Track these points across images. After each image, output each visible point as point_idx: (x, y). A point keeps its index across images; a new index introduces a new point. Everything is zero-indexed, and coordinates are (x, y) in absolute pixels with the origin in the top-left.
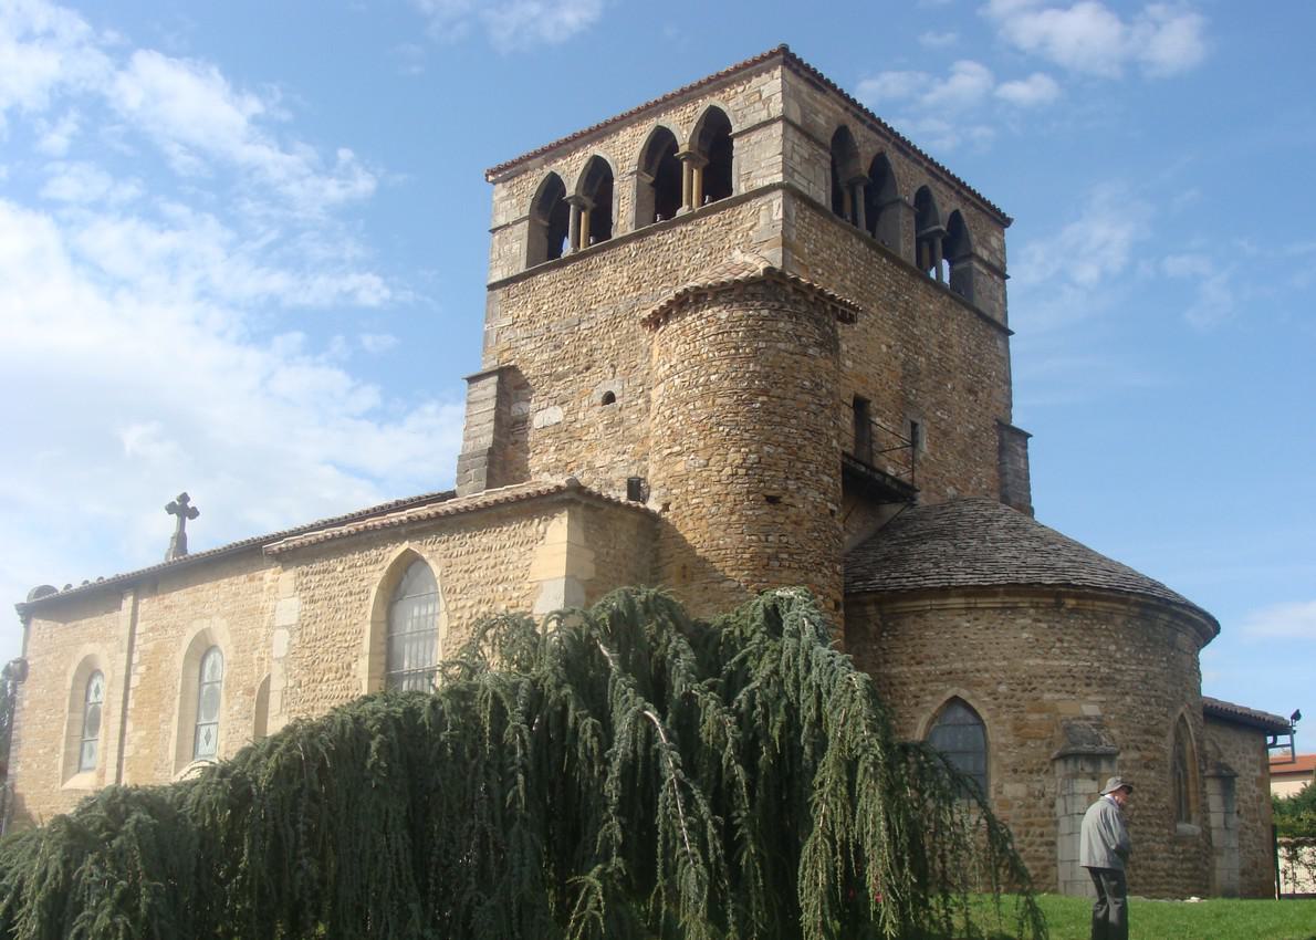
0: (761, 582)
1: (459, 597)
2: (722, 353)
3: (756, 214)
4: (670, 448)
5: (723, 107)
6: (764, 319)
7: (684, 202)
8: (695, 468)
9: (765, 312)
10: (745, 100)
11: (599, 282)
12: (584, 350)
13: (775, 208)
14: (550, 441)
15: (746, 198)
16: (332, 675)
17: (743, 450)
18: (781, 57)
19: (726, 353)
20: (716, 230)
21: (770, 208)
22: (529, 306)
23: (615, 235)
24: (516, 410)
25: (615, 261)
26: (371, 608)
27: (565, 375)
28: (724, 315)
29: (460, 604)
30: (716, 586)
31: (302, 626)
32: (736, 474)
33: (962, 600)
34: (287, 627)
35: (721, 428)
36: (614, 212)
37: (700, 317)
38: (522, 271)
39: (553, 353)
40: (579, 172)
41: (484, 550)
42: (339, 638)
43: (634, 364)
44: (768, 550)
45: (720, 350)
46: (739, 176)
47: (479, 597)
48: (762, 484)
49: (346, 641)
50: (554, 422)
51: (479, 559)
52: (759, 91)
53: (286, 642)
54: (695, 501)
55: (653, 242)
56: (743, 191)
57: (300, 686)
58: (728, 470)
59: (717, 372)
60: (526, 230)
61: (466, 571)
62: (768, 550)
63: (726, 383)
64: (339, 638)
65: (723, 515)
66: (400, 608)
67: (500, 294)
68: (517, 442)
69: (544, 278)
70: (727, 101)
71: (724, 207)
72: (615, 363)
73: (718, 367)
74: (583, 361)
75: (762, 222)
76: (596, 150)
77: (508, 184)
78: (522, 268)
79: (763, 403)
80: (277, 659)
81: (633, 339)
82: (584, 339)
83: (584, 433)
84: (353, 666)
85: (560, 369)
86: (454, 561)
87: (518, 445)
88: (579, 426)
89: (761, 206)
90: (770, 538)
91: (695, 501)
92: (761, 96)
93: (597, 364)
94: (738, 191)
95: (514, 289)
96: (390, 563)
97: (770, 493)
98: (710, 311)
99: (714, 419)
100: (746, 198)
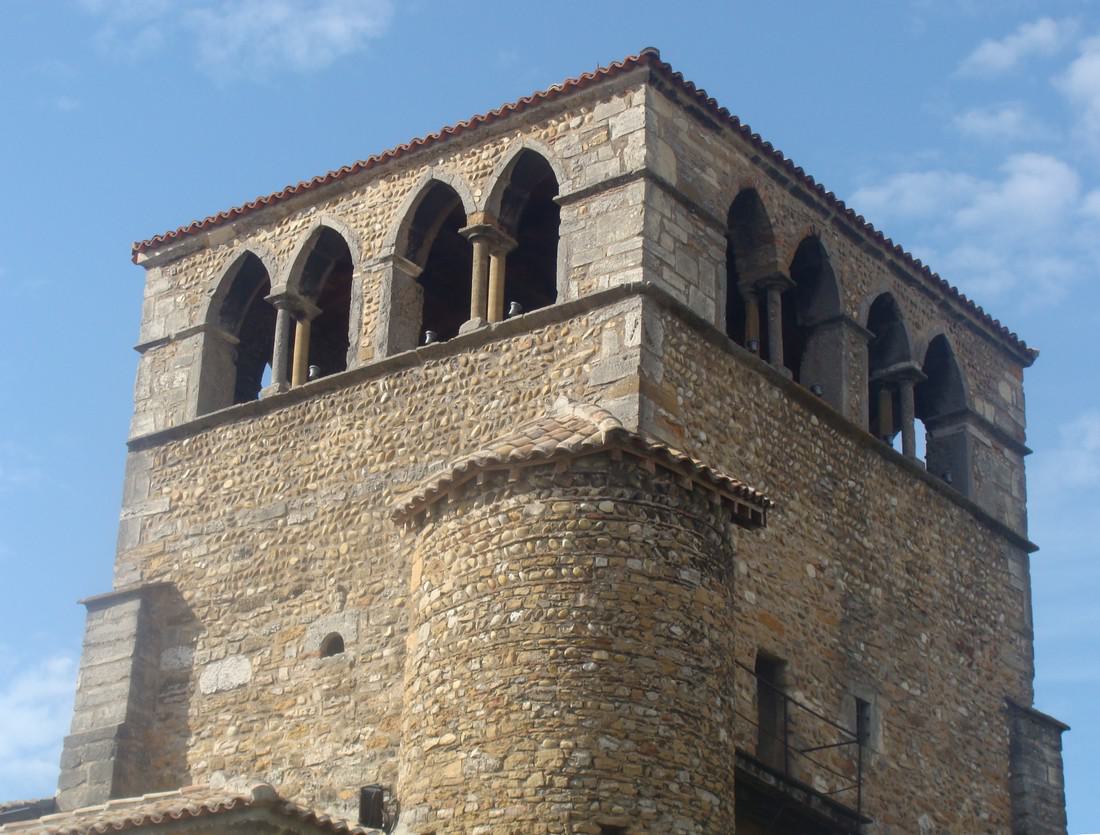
3: (596, 336)
4: (436, 735)
6: (606, 517)
9: (607, 506)
10: (582, 140)
11: (321, 444)
19: (538, 574)
23: (353, 364)
27: (258, 602)
28: (536, 508)
32: (551, 784)
35: (526, 705)
36: (353, 325)
37: (496, 511)
39: (238, 563)
40: (294, 254)
43: (378, 586)
55: (418, 378)
56: (574, 295)
59: (521, 607)
60: (199, 350)
67: (149, 457)
68: (168, 716)
69: (228, 434)
71: (541, 322)
72: (345, 584)
74: (289, 579)
76: (324, 216)
77: (171, 269)
78: (189, 413)
79: (600, 663)
82: (293, 541)
89: (606, 321)
92: (609, 134)
93: (314, 585)
95: (175, 451)
98: (512, 502)
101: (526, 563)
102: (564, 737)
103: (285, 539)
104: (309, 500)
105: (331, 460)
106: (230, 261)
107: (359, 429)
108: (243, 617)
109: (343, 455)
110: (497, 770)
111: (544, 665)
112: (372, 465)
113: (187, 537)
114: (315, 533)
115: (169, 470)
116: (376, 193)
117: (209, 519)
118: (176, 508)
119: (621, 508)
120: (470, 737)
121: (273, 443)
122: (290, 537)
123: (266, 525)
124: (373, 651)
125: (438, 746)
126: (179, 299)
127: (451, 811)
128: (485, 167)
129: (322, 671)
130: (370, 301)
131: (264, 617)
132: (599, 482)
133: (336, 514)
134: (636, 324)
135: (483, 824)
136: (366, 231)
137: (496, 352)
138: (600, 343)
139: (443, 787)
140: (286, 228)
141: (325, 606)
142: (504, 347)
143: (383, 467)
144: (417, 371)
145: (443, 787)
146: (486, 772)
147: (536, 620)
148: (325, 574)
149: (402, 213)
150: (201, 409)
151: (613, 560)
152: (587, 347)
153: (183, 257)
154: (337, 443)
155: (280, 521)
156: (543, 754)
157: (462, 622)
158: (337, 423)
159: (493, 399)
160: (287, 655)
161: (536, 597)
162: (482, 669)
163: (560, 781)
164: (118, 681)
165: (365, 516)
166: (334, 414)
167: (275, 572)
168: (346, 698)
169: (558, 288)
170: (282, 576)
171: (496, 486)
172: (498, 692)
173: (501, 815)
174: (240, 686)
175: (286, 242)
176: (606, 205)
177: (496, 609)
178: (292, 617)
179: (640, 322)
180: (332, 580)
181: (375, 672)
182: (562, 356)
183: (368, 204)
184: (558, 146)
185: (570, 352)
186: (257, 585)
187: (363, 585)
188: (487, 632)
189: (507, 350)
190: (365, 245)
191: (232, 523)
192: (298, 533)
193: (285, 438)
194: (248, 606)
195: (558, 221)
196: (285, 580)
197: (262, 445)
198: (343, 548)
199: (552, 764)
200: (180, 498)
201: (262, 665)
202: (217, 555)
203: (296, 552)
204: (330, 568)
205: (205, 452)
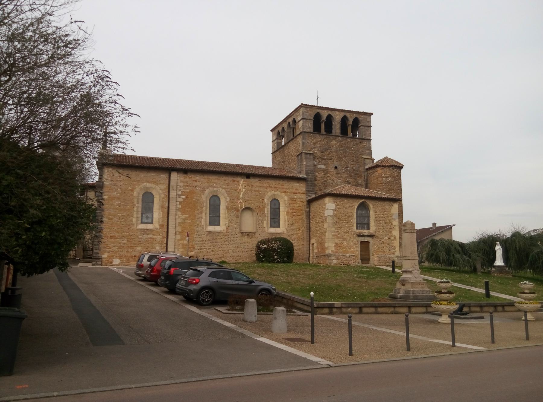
27: (325, 159)
75: (367, 145)
194: (324, 159)
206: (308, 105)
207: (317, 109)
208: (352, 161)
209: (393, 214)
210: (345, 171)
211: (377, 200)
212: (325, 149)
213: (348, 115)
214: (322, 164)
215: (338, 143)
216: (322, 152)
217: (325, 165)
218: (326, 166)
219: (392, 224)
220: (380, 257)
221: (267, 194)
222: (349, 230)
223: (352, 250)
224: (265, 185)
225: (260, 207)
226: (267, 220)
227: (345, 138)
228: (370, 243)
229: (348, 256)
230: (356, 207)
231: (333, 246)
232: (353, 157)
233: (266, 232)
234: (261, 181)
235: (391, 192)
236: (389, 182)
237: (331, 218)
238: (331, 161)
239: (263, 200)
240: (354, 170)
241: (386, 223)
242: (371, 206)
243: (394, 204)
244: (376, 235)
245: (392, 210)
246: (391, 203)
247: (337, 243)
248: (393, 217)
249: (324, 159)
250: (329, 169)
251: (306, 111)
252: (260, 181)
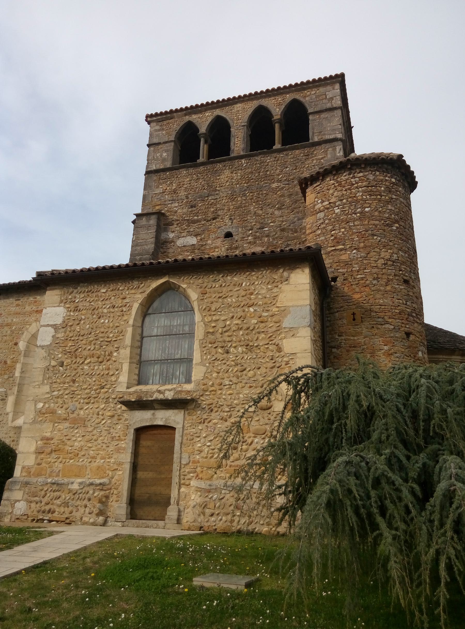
0: (406, 327)
1: (213, 313)
2: (372, 197)
3: (326, 152)
4: (334, 246)
5: (302, 99)
6: (393, 183)
7: (276, 141)
8: (357, 258)
9: (393, 180)
10: (316, 97)
11: (221, 177)
12: (212, 210)
13: (338, 150)
14: (188, 254)
15: (319, 143)
16: (93, 360)
17: (389, 251)
18: (340, 79)
19: (375, 197)
20: (300, 158)
21: (335, 150)
22: (174, 185)
23: (232, 155)
24: (163, 236)
25: (232, 168)
26: (133, 316)
27: (198, 221)
28: (371, 177)
29: (214, 318)
30: (379, 326)
31: (65, 325)
32: (387, 264)
33: (459, 357)
34: (51, 326)
35: (376, 237)
36: (232, 144)
37: (354, 177)
38: (168, 166)
39: (190, 209)
40: (208, 123)
41: (235, 285)
42: (101, 335)
43: (246, 219)
44: (408, 310)
45: (370, 195)
46: (313, 133)
47: (231, 315)
48: (401, 272)
49: (108, 337)
50: (191, 244)
51: (231, 291)
52: (325, 94)
53: (51, 335)
54: (359, 276)
55: (257, 161)
56: (316, 139)
57: (62, 366)
58: (382, 261)
59: (369, 207)
60: (172, 147)
61: (219, 297)
62: (408, 310)
63: (376, 213)
64: (101, 335)
65: (382, 285)
66: (147, 320)
67: (155, 177)
68: (165, 252)
69: (184, 172)
70: (305, 97)
71: (304, 147)
72: (232, 217)
73: (371, 204)
74: (210, 216)
75: (329, 156)
76: (218, 112)
77: (160, 124)
78: (169, 164)
79: (397, 228)
80: (40, 346)
81: (245, 207)
82: (211, 204)
83: (212, 251)
84: (115, 354)
85: (195, 218)
86: (208, 290)
87: (165, 254)
88: (208, 247)
89: (329, 148)
90: (408, 303)
91: (359, 276)
92: (326, 97)
93: (220, 218)
94: (312, 139)
95: (162, 175)
96: (151, 289)
97: (405, 278)
98: (361, 174)
99: (370, 232)
100: (319, 143)
101: (369, 193)
102: (389, 249)
103: (208, 204)
104: (217, 192)
105: (225, 182)
106: (182, 124)
107: (235, 173)
108: (193, 225)
109: (230, 180)
110: (365, 258)
111: (380, 225)
112: (241, 184)
113: (169, 201)
114: (220, 202)
115: (162, 181)
116: (239, 106)
117: (178, 196)
118: (165, 192)
119: (397, 182)
120: (351, 247)
121: (202, 176)
122: (210, 203)
123: (201, 199)
124: (244, 237)
125: (335, 250)
126: (163, 132)
127: (346, 270)
128: (280, 103)
129: (225, 242)
130: (237, 138)
131: (201, 225)
132: (390, 172)
133: (228, 198)
134: (341, 149)
135: (361, 274)
136: (235, 118)
137: (287, 155)
138: (326, 154)
139: (340, 262)
140: (204, 115)
141: (224, 224)
142: (290, 153)
143: (245, 185)
144: (256, 158)
145: (340, 262)
146: (361, 258)
147: (375, 211)
148: (224, 214)
149: (250, 113)
150: (173, 163)
151: (397, 197)
152: (322, 155)
153: (164, 120)
154: (227, 177)
155: (206, 198)
156: (383, 254)
157: (342, 211)
158: (227, 172)
159: (287, 168)
160: (211, 237)
161: (375, 204)
162: (354, 226)
163: (389, 263)
164: (151, 238)
165: (239, 199)
166: (225, 169)
167: (205, 213)
168: (235, 251)
169: (310, 138)
170: (208, 214)
171: (353, 170)
172: (363, 233)
173: (369, 272)
174: (193, 245)
175: (205, 119)
176: (327, 116)
177: (359, 207)
178: (212, 226)
179: (342, 149)
180: (227, 216)
181: (246, 244)
182: (313, 157)
183: (236, 110)
184: (307, 99)
185: (315, 156)
186: (198, 216)
187: (239, 218)
188: (355, 214)
189: (291, 154)
190: (235, 122)
191: (187, 198)
192: (213, 202)
193: (206, 175)
194: (194, 222)
195: (309, 119)
196: (209, 215)
197: (197, 176)
198: (232, 207)
199: (387, 257)
200: (166, 189)
201: (201, 239)
202: (182, 206)
203: (213, 208)
204: (226, 213)
205: (176, 176)
206: (161, 114)
207: (186, 115)
208: (279, 209)
209: (284, 311)
210: (256, 238)
211: (219, 272)
212: (201, 197)
213: (269, 103)
214: (190, 234)
215: (237, 176)
216: (192, 207)
217: (196, 236)
218: (199, 238)
219: (279, 350)
220: (209, 491)
221: (27, 329)
222: (103, 388)
223: (99, 462)
224: (28, 308)
225: (5, 362)
226: (16, 393)
227: (258, 158)
228: (177, 431)
229: (75, 487)
230: (136, 306)
231: (33, 449)
232: (282, 196)
233: (10, 424)
234: (19, 302)
235: (341, 250)
236: (338, 219)
237: (45, 355)
238: (214, 221)
239: (16, 344)
240: (283, 230)
241: (249, 348)
242: (193, 295)
243: (292, 275)
244: (205, 401)
245: (281, 296)
246: (281, 273)
247: (48, 439)
248: (287, 323)
249: (194, 222)
250: (209, 242)
251: (158, 127)
252: (17, 302)
